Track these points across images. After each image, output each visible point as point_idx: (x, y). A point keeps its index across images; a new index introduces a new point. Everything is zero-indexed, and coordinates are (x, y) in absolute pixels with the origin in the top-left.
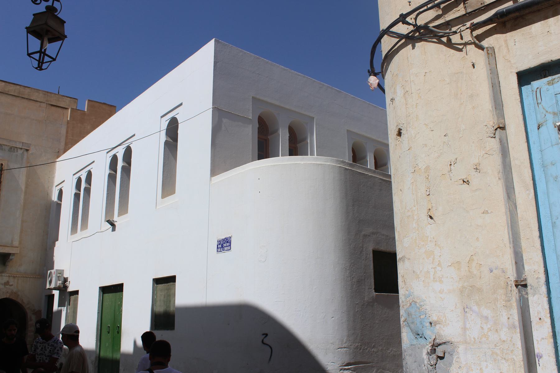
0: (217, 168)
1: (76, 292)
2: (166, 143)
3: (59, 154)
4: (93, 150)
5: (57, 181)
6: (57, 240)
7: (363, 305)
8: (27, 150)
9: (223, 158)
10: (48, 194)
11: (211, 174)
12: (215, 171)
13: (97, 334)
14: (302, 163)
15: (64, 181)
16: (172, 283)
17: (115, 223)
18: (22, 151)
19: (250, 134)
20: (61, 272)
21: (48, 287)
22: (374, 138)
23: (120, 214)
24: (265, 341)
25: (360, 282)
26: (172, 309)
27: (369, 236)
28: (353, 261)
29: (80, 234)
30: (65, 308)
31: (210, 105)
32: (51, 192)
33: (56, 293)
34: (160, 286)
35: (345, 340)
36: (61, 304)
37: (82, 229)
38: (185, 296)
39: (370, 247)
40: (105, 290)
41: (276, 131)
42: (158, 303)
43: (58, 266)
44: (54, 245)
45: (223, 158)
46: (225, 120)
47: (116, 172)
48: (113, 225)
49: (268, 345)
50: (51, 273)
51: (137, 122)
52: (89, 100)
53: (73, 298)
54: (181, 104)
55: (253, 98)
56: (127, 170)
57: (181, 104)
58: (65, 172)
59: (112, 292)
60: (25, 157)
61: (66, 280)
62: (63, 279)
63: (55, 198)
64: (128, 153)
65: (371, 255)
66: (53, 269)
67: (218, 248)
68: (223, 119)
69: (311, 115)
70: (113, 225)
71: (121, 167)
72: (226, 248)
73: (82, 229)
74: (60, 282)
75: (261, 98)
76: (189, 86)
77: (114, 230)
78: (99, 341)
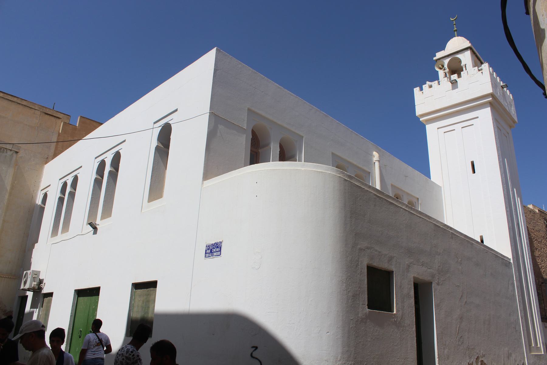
0: (210, 172)
1: (50, 295)
2: (157, 148)
3: (47, 160)
4: (81, 157)
5: (43, 185)
6: (37, 242)
7: (357, 321)
8: (17, 152)
9: (215, 163)
10: (33, 198)
11: (203, 178)
12: (208, 174)
13: (500, 166)
14: (303, 169)
15: (50, 185)
16: (152, 289)
17: (98, 227)
18: (12, 152)
19: (244, 143)
20: (37, 273)
21: (22, 287)
22: (355, 163)
23: (103, 218)
24: (254, 354)
25: (355, 296)
26: (150, 315)
27: (364, 250)
28: (349, 274)
29: (60, 236)
30: (38, 310)
31: (208, 110)
32: (36, 196)
33: (30, 294)
34: (139, 291)
35: (339, 358)
36: (33, 306)
37: (62, 233)
38: (165, 303)
39: (365, 262)
40: (80, 293)
41: (267, 145)
42: (135, 309)
43: (35, 266)
44: (33, 247)
45: (215, 163)
46: (220, 127)
47: (102, 177)
48: (95, 228)
49: (257, 359)
50: (26, 273)
51: (130, 129)
52: (81, 117)
53: (46, 300)
54: (176, 110)
55: (249, 110)
56: (114, 175)
57: (176, 110)
58: (52, 176)
59: (88, 295)
60: (14, 158)
61: (41, 282)
62: (38, 281)
63: (39, 201)
64: (117, 158)
65: (366, 270)
66: (29, 269)
67: (206, 253)
68: (219, 125)
69: (301, 134)
70: (95, 228)
71: (109, 172)
72: (215, 254)
73: (62, 233)
74: (34, 284)
75: (256, 110)
76: (188, 94)
77: (95, 233)
78: (69, 345)
